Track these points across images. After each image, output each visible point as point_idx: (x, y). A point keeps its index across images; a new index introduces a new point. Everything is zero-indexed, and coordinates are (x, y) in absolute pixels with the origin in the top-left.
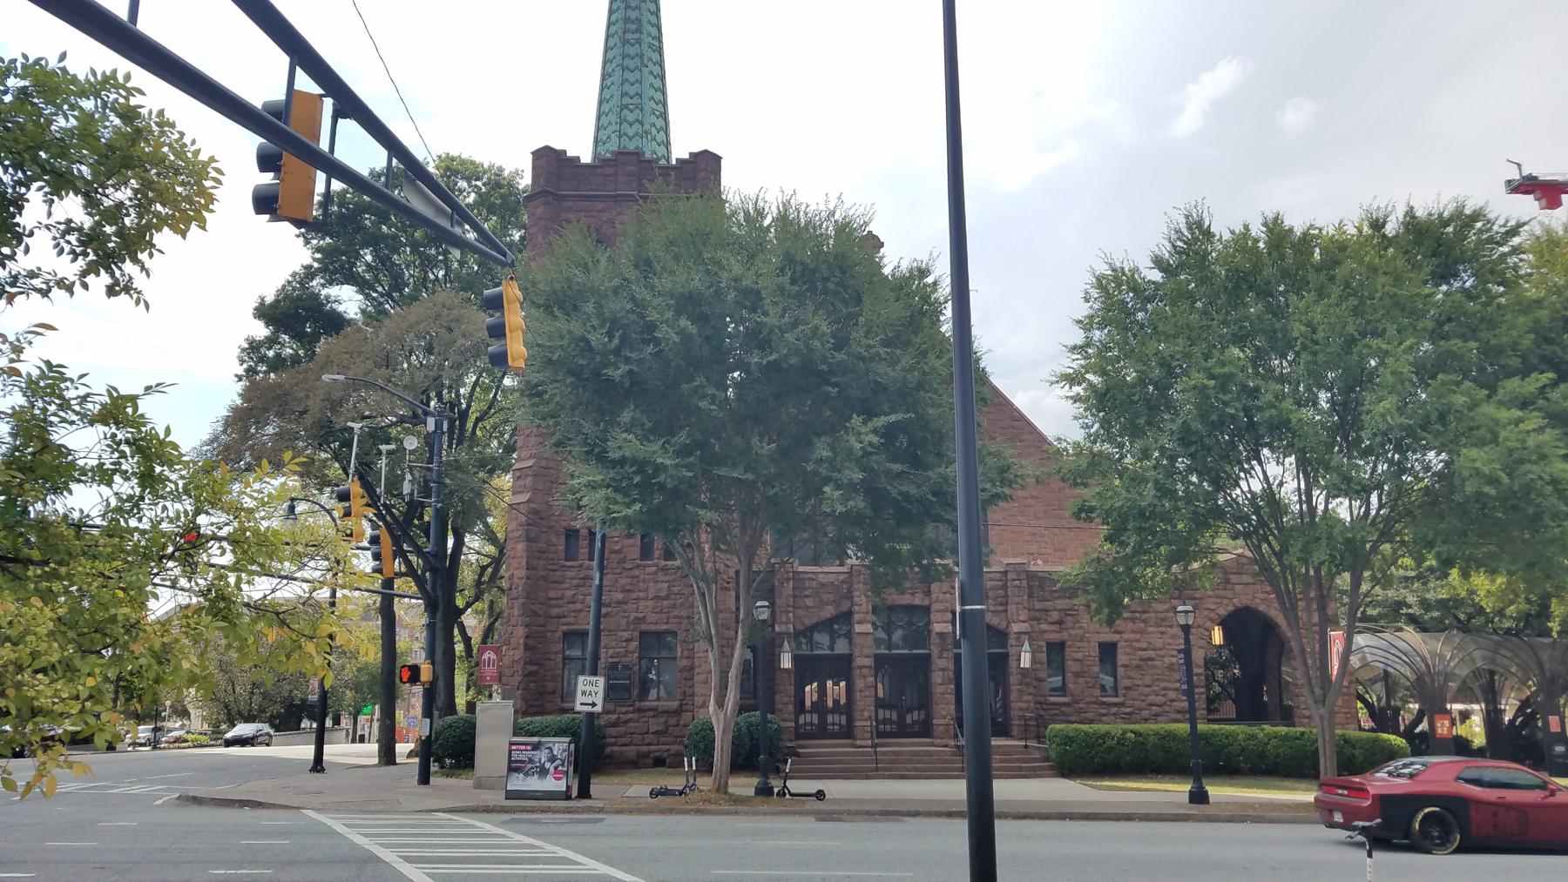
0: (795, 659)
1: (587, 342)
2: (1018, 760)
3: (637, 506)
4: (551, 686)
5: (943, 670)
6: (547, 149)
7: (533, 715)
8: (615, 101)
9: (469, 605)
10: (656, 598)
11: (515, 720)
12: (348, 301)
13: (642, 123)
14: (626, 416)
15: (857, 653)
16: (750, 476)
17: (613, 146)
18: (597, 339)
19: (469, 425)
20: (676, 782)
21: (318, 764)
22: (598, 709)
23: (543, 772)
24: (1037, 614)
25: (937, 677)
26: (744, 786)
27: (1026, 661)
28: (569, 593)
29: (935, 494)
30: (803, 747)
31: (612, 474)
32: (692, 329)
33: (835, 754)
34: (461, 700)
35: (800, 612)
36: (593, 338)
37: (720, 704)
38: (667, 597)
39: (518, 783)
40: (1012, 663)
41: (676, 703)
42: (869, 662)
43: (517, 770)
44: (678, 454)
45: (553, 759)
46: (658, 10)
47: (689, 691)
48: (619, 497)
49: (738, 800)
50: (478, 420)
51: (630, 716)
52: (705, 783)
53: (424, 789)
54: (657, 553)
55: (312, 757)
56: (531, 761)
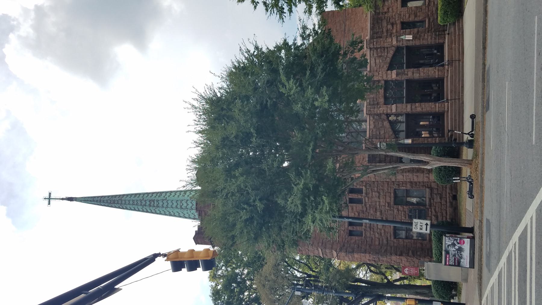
0: (407, 137)
1: (246, 220)
2: (455, 37)
3: (324, 198)
4: (419, 245)
5: (413, 73)
7: (432, 254)
8: (179, 210)
9: (386, 278)
10: (379, 197)
11: (434, 262)
13: (187, 200)
14: (280, 201)
15: (405, 111)
16: (312, 144)
17: (194, 211)
18: (244, 215)
19: (314, 274)
20: (465, 187)
22: (429, 222)
23: (460, 250)
24: (389, 34)
25: (416, 76)
26: (467, 153)
27: (410, 37)
28: (377, 235)
29: (322, 56)
30: (448, 127)
31: (309, 211)
32: (240, 169)
33: (451, 119)
34: (428, 283)
35: (387, 136)
36: (244, 217)
37: (426, 163)
38: (379, 193)
39: (466, 261)
40: (410, 44)
41: (427, 189)
42: (409, 106)
43: (459, 262)
44: (299, 179)
45: (454, 245)
46: (147, 193)
47: (422, 184)
48: (320, 207)
49: (476, 155)
50: (313, 271)
51: (433, 211)
52: (466, 172)
54: (360, 197)
56: (454, 255)
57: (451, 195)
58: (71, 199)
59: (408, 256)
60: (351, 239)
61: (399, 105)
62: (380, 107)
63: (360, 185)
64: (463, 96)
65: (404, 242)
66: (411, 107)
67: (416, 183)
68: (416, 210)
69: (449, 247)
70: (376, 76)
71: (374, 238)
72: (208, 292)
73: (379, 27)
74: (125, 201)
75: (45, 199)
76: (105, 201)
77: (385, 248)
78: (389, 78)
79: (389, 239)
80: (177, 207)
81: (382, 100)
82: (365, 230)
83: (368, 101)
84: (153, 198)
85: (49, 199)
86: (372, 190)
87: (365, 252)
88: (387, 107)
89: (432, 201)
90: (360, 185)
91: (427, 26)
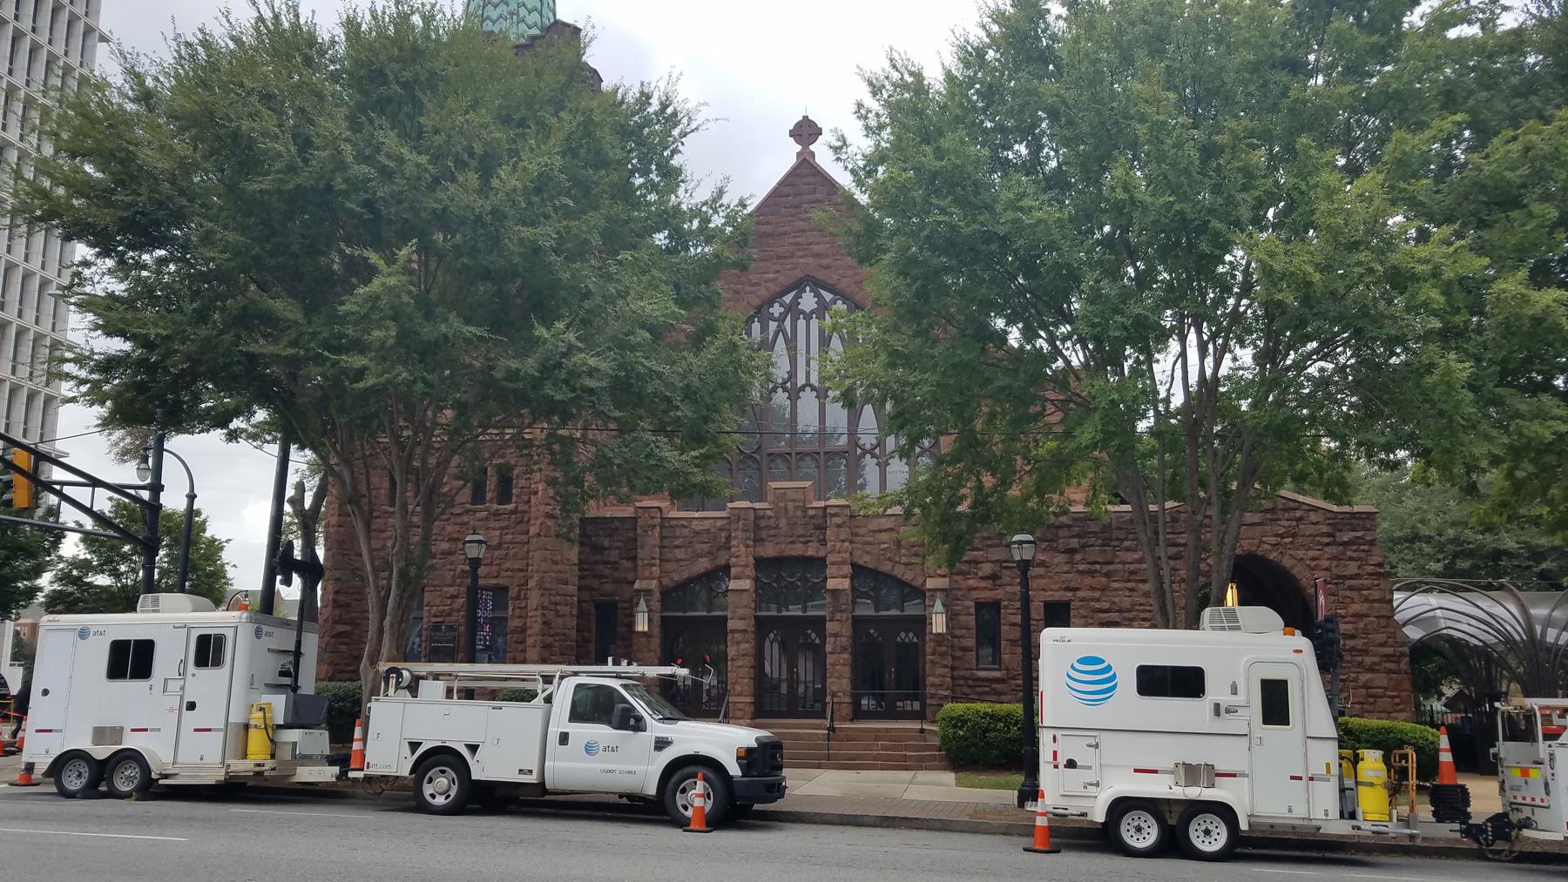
5: (836, 635)
35: (669, 566)
42: (748, 625)
59: (335, 622)
62: (747, 546)
67: (523, 642)
68: (453, 640)
70: (837, 535)
73: (989, 538)
81: (769, 551)
88: (747, 566)
91: (982, 674)
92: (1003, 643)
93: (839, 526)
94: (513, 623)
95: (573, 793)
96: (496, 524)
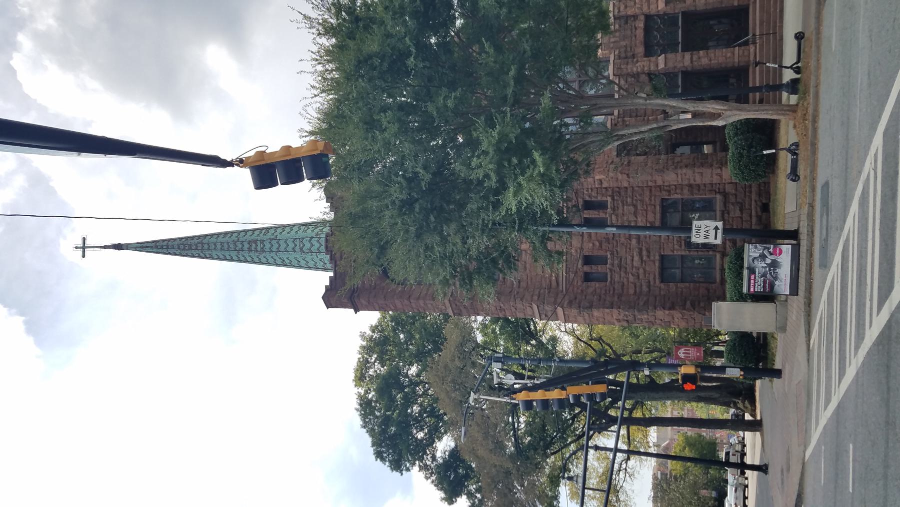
6: (324, 298)
8: (298, 256)
10: (635, 214)
12: (444, 445)
13: (311, 238)
20: (785, 161)
21: (762, 469)
23: (774, 265)
28: (631, 278)
38: (635, 206)
41: (718, 197)
42: (687, 56)
45: (763, 257)
53: (785, 374)
54: (602, 215)
55: (756, 473)
56: (764, 275)
57: (759, 203)
58: (118, 247)
59: (684, 309)
60: (588, 287)
61: (670, 56)
62: (638, 61)
63: (603, 195)
64: (781, 27)
65: (677, 287)
66: (692, 58)
67: (698, 186)
69: (756, 262)
71: (626, 283)
72: (354, 403)
74: (208, 244)
75: (76, 248)
76: (176, 247)
77: (645, 299)
78: (653, 11)
79: (652, 283)
80: (294, 250)
81: (640, 50)
82: (611, 270)
83: (617, 53)
84: (254, 237)
85: (84, 248)
86: (622, 202)
87: (611, 306)
88: (650, 61)
89: (726, 215)
90: (603, 195)
92: (741, 433)
93: (626, 7)
94: (686, 195)
95: (818, 48)
96: (621, 208)
